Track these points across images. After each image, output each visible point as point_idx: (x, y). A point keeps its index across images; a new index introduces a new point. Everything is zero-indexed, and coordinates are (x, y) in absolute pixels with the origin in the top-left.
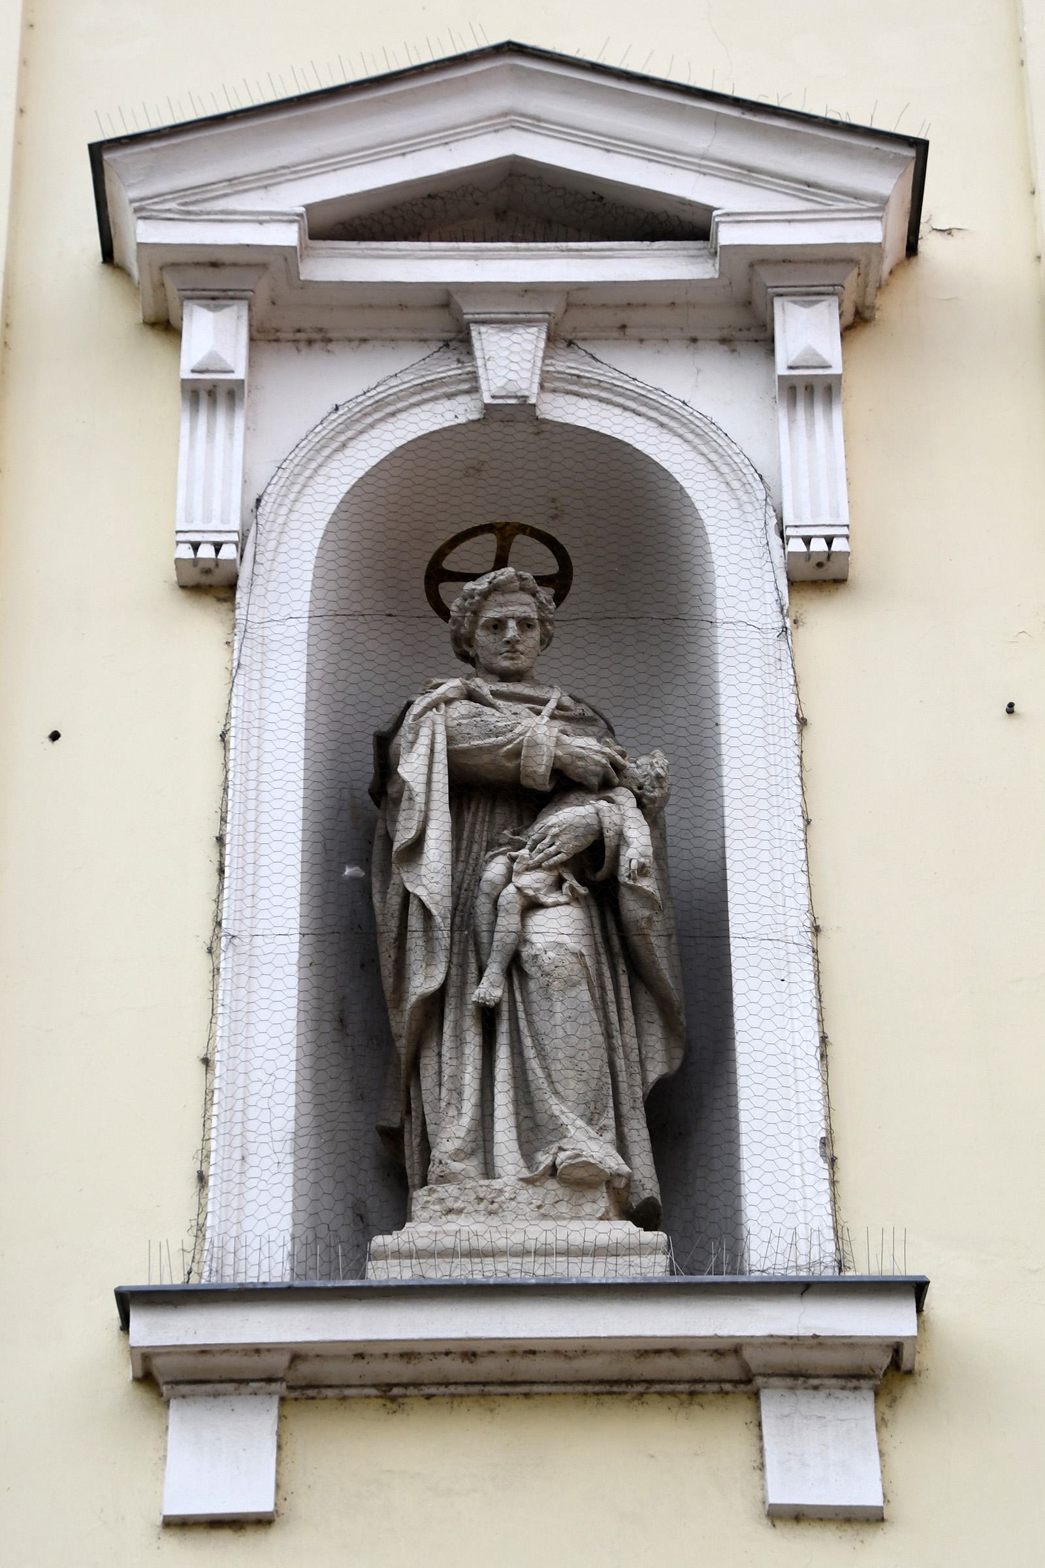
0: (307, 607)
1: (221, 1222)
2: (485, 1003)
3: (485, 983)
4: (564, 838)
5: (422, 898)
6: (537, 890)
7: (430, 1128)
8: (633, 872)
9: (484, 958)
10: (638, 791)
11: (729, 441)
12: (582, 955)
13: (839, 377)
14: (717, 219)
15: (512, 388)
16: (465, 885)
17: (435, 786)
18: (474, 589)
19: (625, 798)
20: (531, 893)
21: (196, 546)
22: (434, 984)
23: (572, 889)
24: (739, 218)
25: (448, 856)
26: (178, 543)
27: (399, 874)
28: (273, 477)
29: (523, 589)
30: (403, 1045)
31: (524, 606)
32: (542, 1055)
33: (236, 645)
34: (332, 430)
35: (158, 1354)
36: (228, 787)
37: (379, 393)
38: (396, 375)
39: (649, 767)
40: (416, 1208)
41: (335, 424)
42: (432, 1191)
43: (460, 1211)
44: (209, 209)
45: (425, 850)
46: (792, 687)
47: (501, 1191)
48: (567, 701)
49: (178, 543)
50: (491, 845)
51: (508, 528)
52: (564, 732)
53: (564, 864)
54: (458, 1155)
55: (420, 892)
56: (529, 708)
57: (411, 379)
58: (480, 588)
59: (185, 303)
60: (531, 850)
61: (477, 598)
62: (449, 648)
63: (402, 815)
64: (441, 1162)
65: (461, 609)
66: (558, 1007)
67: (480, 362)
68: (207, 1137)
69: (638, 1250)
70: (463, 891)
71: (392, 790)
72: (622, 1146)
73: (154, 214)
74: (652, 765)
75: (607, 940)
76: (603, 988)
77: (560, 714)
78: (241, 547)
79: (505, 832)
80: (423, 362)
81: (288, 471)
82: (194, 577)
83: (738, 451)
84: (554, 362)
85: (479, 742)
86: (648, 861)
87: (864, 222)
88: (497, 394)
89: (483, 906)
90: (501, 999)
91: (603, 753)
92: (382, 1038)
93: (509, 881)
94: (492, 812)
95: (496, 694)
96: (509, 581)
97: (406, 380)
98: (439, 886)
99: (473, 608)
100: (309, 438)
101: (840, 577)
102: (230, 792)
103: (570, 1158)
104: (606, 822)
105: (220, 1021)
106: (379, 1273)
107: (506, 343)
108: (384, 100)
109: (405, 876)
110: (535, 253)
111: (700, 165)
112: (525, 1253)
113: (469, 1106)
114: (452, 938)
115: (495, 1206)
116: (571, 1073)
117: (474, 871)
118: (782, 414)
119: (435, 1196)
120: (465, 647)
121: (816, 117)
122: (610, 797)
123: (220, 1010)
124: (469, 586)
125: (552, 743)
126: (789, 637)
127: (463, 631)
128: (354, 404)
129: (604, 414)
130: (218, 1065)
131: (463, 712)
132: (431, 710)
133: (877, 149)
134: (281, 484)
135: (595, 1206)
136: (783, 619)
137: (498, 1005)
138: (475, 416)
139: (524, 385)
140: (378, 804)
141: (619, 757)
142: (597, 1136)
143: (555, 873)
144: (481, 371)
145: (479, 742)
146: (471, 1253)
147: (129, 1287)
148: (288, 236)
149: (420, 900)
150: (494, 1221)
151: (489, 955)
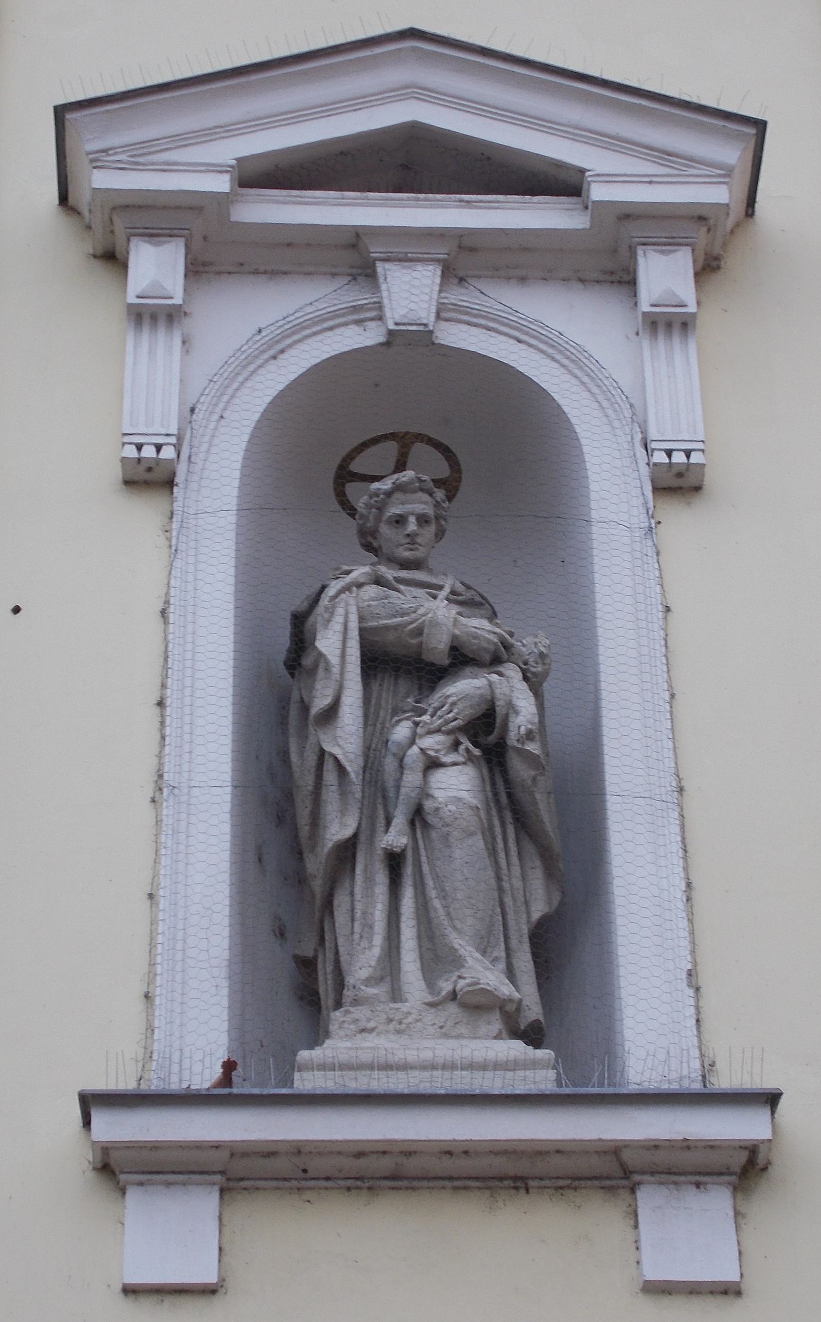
0: (235, 501)
1: (166, 1036)
2: (392, 850)
3: (393, 832)
4: (460, 705)
5: (337, 756)
6: (437, 751)
7: (343, 959)
8: (522, 737)
9: (391, 810)
10: (524, 667)
11: (599, 367)
12: (478, 808)
13: (693, 316)
14: (589, 179)
15: (412, 317)
16: (373, 746)
17: (348, 659)
18: (379, 489)
19: (512, 672)
20: (432, 753)
21: (139, 447)
22: (348, 832)
23: (468, 750)
24: (609, 179)
25: (361, 720)
26: (124, 444)
27: (316, 735)
28: (205, 389)
29: (422, 490)
30: (318, 886)
31: (421, 504)
32: (444, 896)
33: (174, 533)
34: (257, 349)
35: (115, 1148)
36: (168, 657)
37: (297, 318)
38: (311, 304)
39: (533, 646)
40: (333, 1027)
41: (259, 344)
42: (347, 1012)
43: (372, 1030)
44: (155, 161)
45: (340, 714)
46: (657, 579)
47: (409, 1013)
48: (460, 588)
49: (124, 444)
50: (395, 712)
51: (407, 437)
52: (460, 614)
53: (460, 729)
54: (369, 981)
55: (336, 751)
56: (428, 593)
57: (324, 306)
58: (386, 487)
59: (132, 238)
60: (432, 716)
61: (382, 496)
62: (356, 540)
63: (319, 685)
64: (354, 987)
65: (368, 506)
66: (457, 854)
67: (385, 294)
68: (152, 962)
69: (534, 1065)
70: (372, 751)
71: (307, 661)
72: (511, 974)
73: (107, 164)
74: (536, 644)
75: (496, 794)
76: (494, 838)
77: (454, 598)
78: (178, 447)
79: (409, 700)
80: (334, 293)
81: (218, 383)
82: (140, 473)
83: (607, 376)
84: (448, 295)
85: (386, 621)
86: (534, 727)
87: (713, 186)
88: (399, 321)
89: (390, 764)
90: (406, 846)
91: (495, 633)
92: (301, 879)
93: (412, 742)
94: (396, 684)
95: (399, 580)
96: (411, 482)
97: (320, 308)
98: (353, 746)
99: (379, 505)
100: (236, 356)
101: (697, 485)
102: (170, 660)
103: (469, 985)
104: (498, 692)
105: (163, 861)
106: (304, 1082)
107: (407, 278)
108: (305, 73)
109: (322, 737)
110: (433, 203)
111: (573, 134)
112: (433, 1067)
113: (378, 939)
114: (363, 792)
115: (403, 1026)
116: (468, 912)
117: (381, 734)
118: (646, 344)
119: (352, 1016)
120: (370, 539)
121: (672, 98)
122: (500, 671)
123: (163, 851)
124: (376, 485)
125: (450, 624)
126: (654, 535)
127: (369, 525)
128: (276, 328)
129: (492, 341)
130: (162, 900)
131: (373, 595)
132: (344, 593)
133: (724, 126)
134: (212, 394)
135: (490, 1027)
136: (649, 520)
137: (404, 851)
138: (382, 339)
139: (423, 314)
140: (292, 675)
141: (507, 636)
142: (491, 966)
143: (452, 737)
144: (386, 302)
145: (386, 621)
146: (387, 1067)
147: (99, 1090)
148: (221, 184)
149: (336, 759)
150: (404, 1040)
151: (396, 806)
